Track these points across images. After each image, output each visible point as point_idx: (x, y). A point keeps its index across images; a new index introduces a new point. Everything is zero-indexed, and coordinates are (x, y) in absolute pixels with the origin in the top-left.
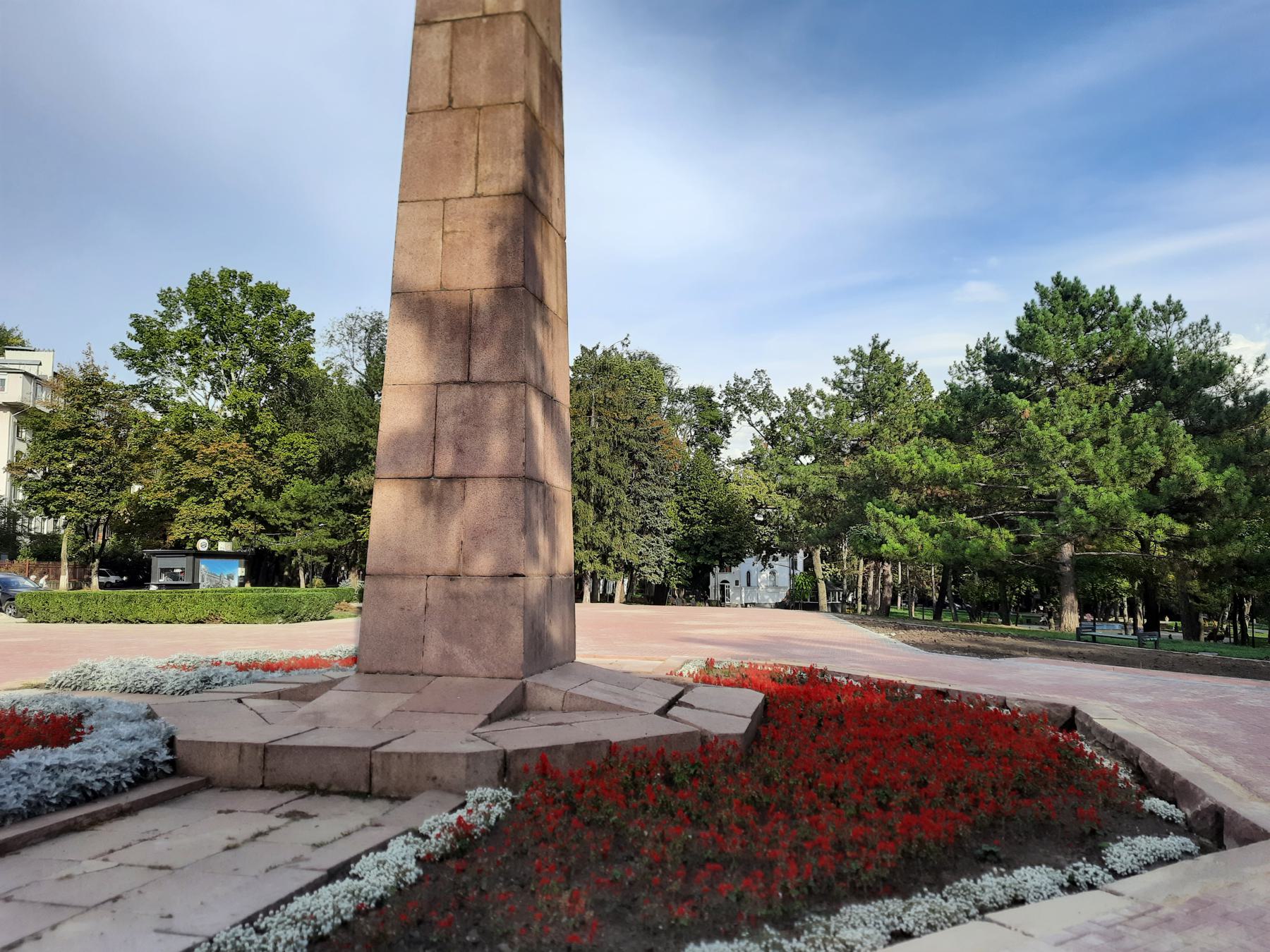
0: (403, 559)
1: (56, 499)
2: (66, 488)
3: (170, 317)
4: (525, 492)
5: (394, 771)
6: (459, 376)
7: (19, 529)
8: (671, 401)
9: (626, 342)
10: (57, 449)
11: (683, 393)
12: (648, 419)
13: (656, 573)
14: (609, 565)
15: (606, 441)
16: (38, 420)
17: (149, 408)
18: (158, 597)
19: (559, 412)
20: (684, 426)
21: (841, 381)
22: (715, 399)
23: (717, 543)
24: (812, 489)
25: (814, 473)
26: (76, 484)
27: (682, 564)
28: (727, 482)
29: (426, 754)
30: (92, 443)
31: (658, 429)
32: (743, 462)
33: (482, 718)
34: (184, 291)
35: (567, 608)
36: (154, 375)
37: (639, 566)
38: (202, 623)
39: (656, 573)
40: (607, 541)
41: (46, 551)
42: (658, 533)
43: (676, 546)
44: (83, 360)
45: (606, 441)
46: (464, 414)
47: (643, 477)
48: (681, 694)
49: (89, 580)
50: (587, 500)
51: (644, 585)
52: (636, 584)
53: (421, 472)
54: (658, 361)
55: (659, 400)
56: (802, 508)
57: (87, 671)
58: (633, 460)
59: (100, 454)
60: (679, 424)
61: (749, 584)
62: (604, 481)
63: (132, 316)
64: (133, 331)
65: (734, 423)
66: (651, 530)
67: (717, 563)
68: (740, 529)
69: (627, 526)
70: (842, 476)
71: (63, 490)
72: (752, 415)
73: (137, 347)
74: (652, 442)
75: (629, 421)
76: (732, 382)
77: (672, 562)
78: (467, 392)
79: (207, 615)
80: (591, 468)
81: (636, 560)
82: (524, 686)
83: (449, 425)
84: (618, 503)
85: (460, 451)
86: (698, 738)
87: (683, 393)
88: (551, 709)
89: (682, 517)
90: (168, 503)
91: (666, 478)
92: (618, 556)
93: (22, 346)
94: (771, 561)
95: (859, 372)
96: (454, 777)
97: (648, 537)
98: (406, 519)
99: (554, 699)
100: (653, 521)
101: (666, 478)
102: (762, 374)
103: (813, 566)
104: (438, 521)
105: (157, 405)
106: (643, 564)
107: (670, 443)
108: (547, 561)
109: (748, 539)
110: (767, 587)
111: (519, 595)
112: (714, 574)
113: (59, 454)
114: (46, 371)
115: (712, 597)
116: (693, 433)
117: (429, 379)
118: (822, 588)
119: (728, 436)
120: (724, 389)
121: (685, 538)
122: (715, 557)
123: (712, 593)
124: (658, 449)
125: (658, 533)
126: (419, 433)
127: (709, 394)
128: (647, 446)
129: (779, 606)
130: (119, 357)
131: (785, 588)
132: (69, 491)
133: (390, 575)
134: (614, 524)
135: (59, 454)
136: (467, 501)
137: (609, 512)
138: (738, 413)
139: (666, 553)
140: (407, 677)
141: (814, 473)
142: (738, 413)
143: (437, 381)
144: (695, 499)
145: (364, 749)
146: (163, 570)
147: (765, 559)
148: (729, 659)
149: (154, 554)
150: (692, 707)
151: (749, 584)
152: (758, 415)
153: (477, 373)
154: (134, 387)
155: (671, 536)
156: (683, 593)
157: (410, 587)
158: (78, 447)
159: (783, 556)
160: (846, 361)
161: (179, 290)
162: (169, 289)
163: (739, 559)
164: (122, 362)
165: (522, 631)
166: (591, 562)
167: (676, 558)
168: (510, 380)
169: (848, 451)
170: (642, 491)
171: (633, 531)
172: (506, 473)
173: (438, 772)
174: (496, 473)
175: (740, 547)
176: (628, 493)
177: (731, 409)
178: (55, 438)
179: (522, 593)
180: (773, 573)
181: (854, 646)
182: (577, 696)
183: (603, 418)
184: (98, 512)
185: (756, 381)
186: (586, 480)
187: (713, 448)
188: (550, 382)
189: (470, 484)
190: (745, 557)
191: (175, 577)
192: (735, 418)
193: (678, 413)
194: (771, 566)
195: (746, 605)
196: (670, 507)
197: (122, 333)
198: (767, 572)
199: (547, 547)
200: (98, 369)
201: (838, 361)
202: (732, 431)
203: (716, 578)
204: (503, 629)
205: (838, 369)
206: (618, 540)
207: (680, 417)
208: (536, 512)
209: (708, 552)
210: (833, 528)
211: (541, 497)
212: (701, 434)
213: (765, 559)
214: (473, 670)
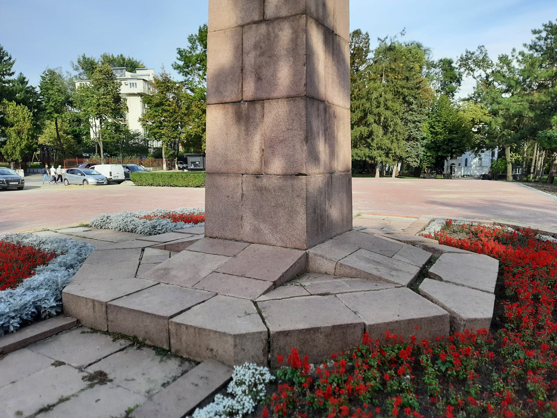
0: (226, 162)
1: (158, 133)
2: (161, 128)
3: (193, 48)
4: (307, 108)
5: (184, 338)
6: (256, 18)
7: (149, 146)
8: (428, 68)
9: (403, 33)
10: (156, 112)
11: (435, 63)
12: (415, 77)
13: (415, 161)
14: (390, 158)
15: (390, 91)
16: (148, 99)
17: (189, 92)
18: (181, 175)
19: (339, 45)
20: (435, 81)
21: (535, 45)
22: (453, 65)
23: (450, 144)
24: (512, 111)
25: (514, 102)
26: (164, 126)
27: (430, 156)
28: (458, 111)
29: (205, 330)
30: (168, 108)
31: (420, 82)
32: (468, 100)
33: (269, 284)
34: (198, 35)
35: (345, 195)
36: (189, 76)
37: (406, 158)
38: (199, 187)
39: (415, 161)
40: (389, 146)
41: (158, 155)
42: (417, 140)
43: (428, 147)
44: (161, 71)
45: (390, 91)
46: (261, 48)
47: (410, 110)
48: (430, 262)
49: (175, 166)
50: (379, 124)
51: (409, 166)
52: (405, 166)
53: (234, 98)
54: (421, 46)
55: (421, 67)
56: (504, 123)
57: (105, 219)
58: (405, 101)
59: (172, 113)
60: (432, 81)
61: (466, 165)
62: (388, 113)
63: (177, 49)
64: (179, 56)
65: (463, 78)
66: (413, 138)
67: (450, 155)
68: (464, 136)
69: (400, 137)
70: (531, 102)
71: (160, 129)
72: (475, 72)
73: (181, 63)
74: (416, 90)
75: (404, 79)
76: (464, 54)
77: (424, 155)
78: (263, 28)
79: (200, 184)
80: (381, 106)
81: (404, 155)
82: (307, 255)
83: (250, 59)
84: (396, 124)
85: (259, 79)
86: (447, 320)
87: (435, 63)
88: (326, 273)
89: (431, 131)
90: (199, 133)
91: (423, 110)
92: (395, 153)
93: (143, 68)
94: (480, 153)
95: (548, 38)
96: (226, 352)
97: (412, 142)
98: (227, 134)
99: (328, 266)
100: (414, 133)
101: (423, 110)
102: (482, 48)
103: (505, 155)
104: (247, 134)
105: (192, 90)
106: (409, 157)
107: (426, 91)
108: (328, 162)
109: (469, 141)
110: (476, 167)
111: (302, 189)
112: (447, 160)
113: (157, 114)
114: (151, 78)
115: (445, 172)
116: (440, 85)
117: (237, 23)
118: (510, 167)
119: (460, 86)
120: (459, 58)
121: (432, 142)
122: (448, 152)
123: (445, 170)
124: (419, 94)
125: (417, 140)
126: (232, 67)
127: (450, 62)
128: (413, 92)
129: (484, 177)
130: (175, 69)
131: (487, 167)
132: (162, 129)
133: (220, 174)
134: (393, 136)
135: (157, 114)
136: (266, 119)
137: (391, 130)
138: (467, 72)
139: (421, 151)
140: (233, 242)
141: (514, 102)
142: (467, 72)
143: (242, 23)
144: (439, 121)
145: (164, 318)
146: (192, 163)
147: (476, 152)
148: (461, 218)
149: (188, 156)
150: (441, 279)
151: (466, 165)
152: (479, 72)
153: (270, 12)
154: (182, 82)
155: (424, 141)
156: (429, 171)
157: (232, 181)
158: (164, 111)
159: (487, 150)
160: (540, 32)
161: (196, 35)
162: (192, 35)
163: (462, 152)
164: (176, 71)
165: (305, 216)
166: (380, 156)
167: (427, 153)
168: (294, 13)
169: (535, 88)
170: (409, 118)
171: (403, 139)
172: (292, 94)
173: (213, 345)
174: (285, 94)
175: (464, 146)
176: (402, 119)
177: (462, 70)
178: (155, 107)
179: (305, 187)
180: (480, 159)
181: (547, 208)
182: (345, 266)
183: (389, 78)
184: (174, 138)
185: (478, 53)
186: (379, 113)
187: (451, 92)
188: (331, 18)
189: (267, 105)
190: (466, 151)
191: (196, 165)
192: (464, 76)
193: (432, 75)
194: (480, 156)
195: (464, 176)
196: (424, 126)
197: (174, 58)
198: (477, 159)
199: (327, 152)
200: (167, 75)
201: (535, 32)
202: (462, 82)
203: (447, 164)
204: (292, 214)
205: (534, 37)
206: (395, 145)
207: (433, 77)
208: (316, 124)
209: (444, 149)
210: (524, 134)
211: (322, 113)
212: (444, 85)
213: (476, 152)
214: (273, 241)
